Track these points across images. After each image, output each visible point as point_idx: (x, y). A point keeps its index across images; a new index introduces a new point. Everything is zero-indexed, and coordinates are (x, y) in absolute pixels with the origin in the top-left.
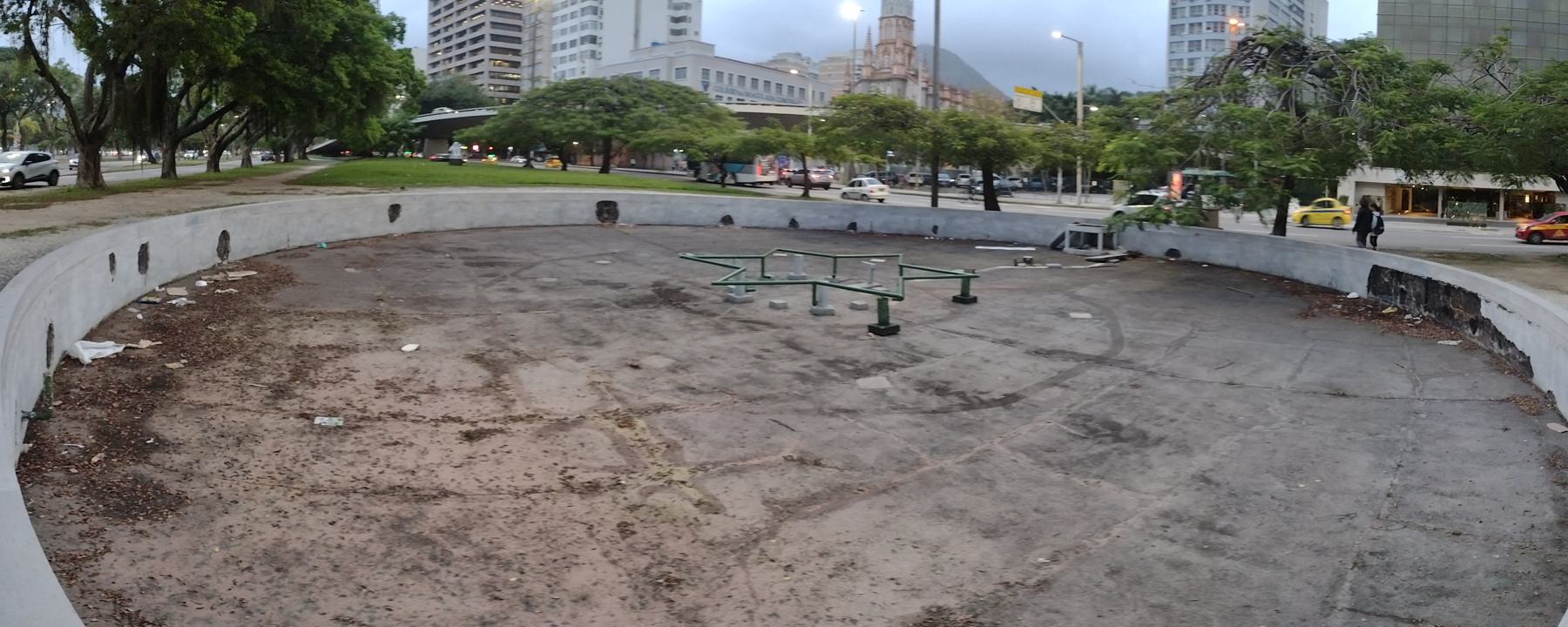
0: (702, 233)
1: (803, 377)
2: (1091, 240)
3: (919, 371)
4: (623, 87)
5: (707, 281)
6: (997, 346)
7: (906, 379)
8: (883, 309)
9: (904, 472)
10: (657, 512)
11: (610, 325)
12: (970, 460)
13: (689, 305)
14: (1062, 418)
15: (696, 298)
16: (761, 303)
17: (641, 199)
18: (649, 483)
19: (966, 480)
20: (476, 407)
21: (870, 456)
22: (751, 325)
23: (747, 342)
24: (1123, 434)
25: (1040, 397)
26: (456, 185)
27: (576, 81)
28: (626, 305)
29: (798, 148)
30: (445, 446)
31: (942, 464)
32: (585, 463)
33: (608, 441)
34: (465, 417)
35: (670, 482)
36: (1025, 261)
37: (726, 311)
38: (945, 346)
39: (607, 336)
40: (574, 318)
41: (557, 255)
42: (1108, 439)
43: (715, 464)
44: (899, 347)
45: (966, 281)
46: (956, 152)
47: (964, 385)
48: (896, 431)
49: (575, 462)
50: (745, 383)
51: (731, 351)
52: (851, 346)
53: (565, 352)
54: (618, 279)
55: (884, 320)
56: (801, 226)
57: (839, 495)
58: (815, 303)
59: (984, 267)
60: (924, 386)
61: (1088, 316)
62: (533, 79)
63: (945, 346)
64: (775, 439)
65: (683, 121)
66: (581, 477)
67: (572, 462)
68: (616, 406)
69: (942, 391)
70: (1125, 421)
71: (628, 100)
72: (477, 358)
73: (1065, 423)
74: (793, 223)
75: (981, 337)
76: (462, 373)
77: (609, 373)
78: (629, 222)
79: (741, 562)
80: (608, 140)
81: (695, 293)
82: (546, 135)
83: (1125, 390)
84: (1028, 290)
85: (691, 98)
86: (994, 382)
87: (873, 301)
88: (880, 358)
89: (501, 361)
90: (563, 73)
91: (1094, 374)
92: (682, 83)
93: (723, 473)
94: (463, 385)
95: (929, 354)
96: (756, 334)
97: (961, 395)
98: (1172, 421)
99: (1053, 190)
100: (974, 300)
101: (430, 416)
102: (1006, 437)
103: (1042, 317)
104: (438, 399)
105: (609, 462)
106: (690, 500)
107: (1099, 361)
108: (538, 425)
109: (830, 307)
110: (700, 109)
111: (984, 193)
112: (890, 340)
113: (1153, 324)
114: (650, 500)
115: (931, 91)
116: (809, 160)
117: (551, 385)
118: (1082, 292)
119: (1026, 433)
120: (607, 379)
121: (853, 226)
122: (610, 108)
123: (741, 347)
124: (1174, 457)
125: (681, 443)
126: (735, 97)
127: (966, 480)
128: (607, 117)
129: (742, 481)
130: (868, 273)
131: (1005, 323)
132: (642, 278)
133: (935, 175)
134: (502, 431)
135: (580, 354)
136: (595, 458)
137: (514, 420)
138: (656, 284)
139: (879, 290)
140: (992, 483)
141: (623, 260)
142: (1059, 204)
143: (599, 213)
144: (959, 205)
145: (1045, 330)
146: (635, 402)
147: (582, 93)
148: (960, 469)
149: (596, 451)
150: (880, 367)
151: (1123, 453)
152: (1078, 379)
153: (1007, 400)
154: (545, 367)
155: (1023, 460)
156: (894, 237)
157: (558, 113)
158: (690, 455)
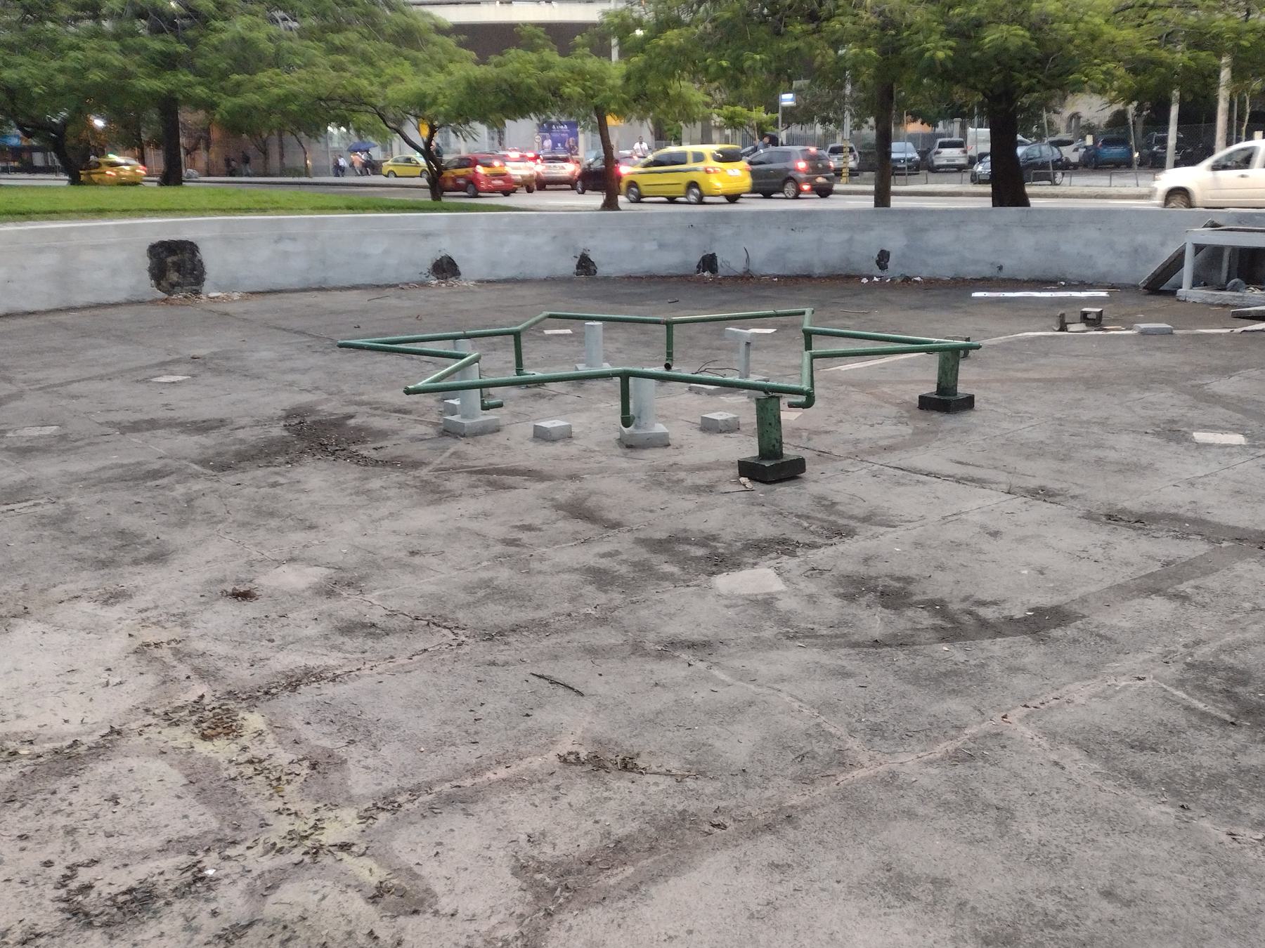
0: (391, 300)
1: (601, 578)
3: (843, 556)
6: (1018, 501)
7: (815, 572)
9: (805, 780)
11: (186, 513)
12: (957, 758)
13: (366, 451)
14: (1173, 671)
15: (382, 434)
16: (515, 433)
17: (244, 237)
18: (268, 863)
21: (738, 744)
22: (495, 478)
25: (1121, 618)
28: (221, 465)
31: (892, 764)
32: (121, 844)
33: (176, 778)
35: (316, 851)
36: (1085, 317)
37: (447, 459)
38: (905, 501)
39: (178, 538)
40: (94, 510)
41: (57, 375)
43: (414, 792)
45: (952, 357)
47: (941, 586)
51: (454, 535)
52: (701, 507)
53: (73, 588)
54: (207, 410)
55: (770, 448)
56: (602, 271)
58: (626, 422)
60: (855, 588)
61: (1238, 439)
63: (905, 501)
64: (543, 717)
66: (111, 881)
68: (199, 689)
69: (894, 596)
73: (1181, 684)
74: (585, 265)
75: (981, 482)
77: (183, 619)
81: (378, 423)
84: (1093, 383)
86: (1011, 580)
87: (740, 408)
88: (763, 529)
95: (867, 519)
96: (507, 496)
97: (937, 606)
100: (968, 403)
102: (1041, 710)
103: (1125, 441)
105: (178, 828)
106: (359, 888)
109: (660, 428)
111: (994, 179)
112: (784, 493)
114: (271, 909)
118: (1221, 386)
119: (1085, 700)
120: (178, 632)
121: (709, 262)
123: (475, 525)
125: (342, 753)
128: (156, 45)
129: (472, 823)
131: (1036, 451)
132: (258, 403)
133: (885, 139)
135: (111, 586)
138: (289, 414)
140: (1004, 816)
141: (217, 371)
143: (158, 273)
144: (946, 202)
146: (242, 675)
148: (932, 777)
150: (761, 548)
152: (1213, 582)
153: (1041, 623)
155: (1077, 764)
156: (797, 281)
157: (37, 42)
158: (362, 781)
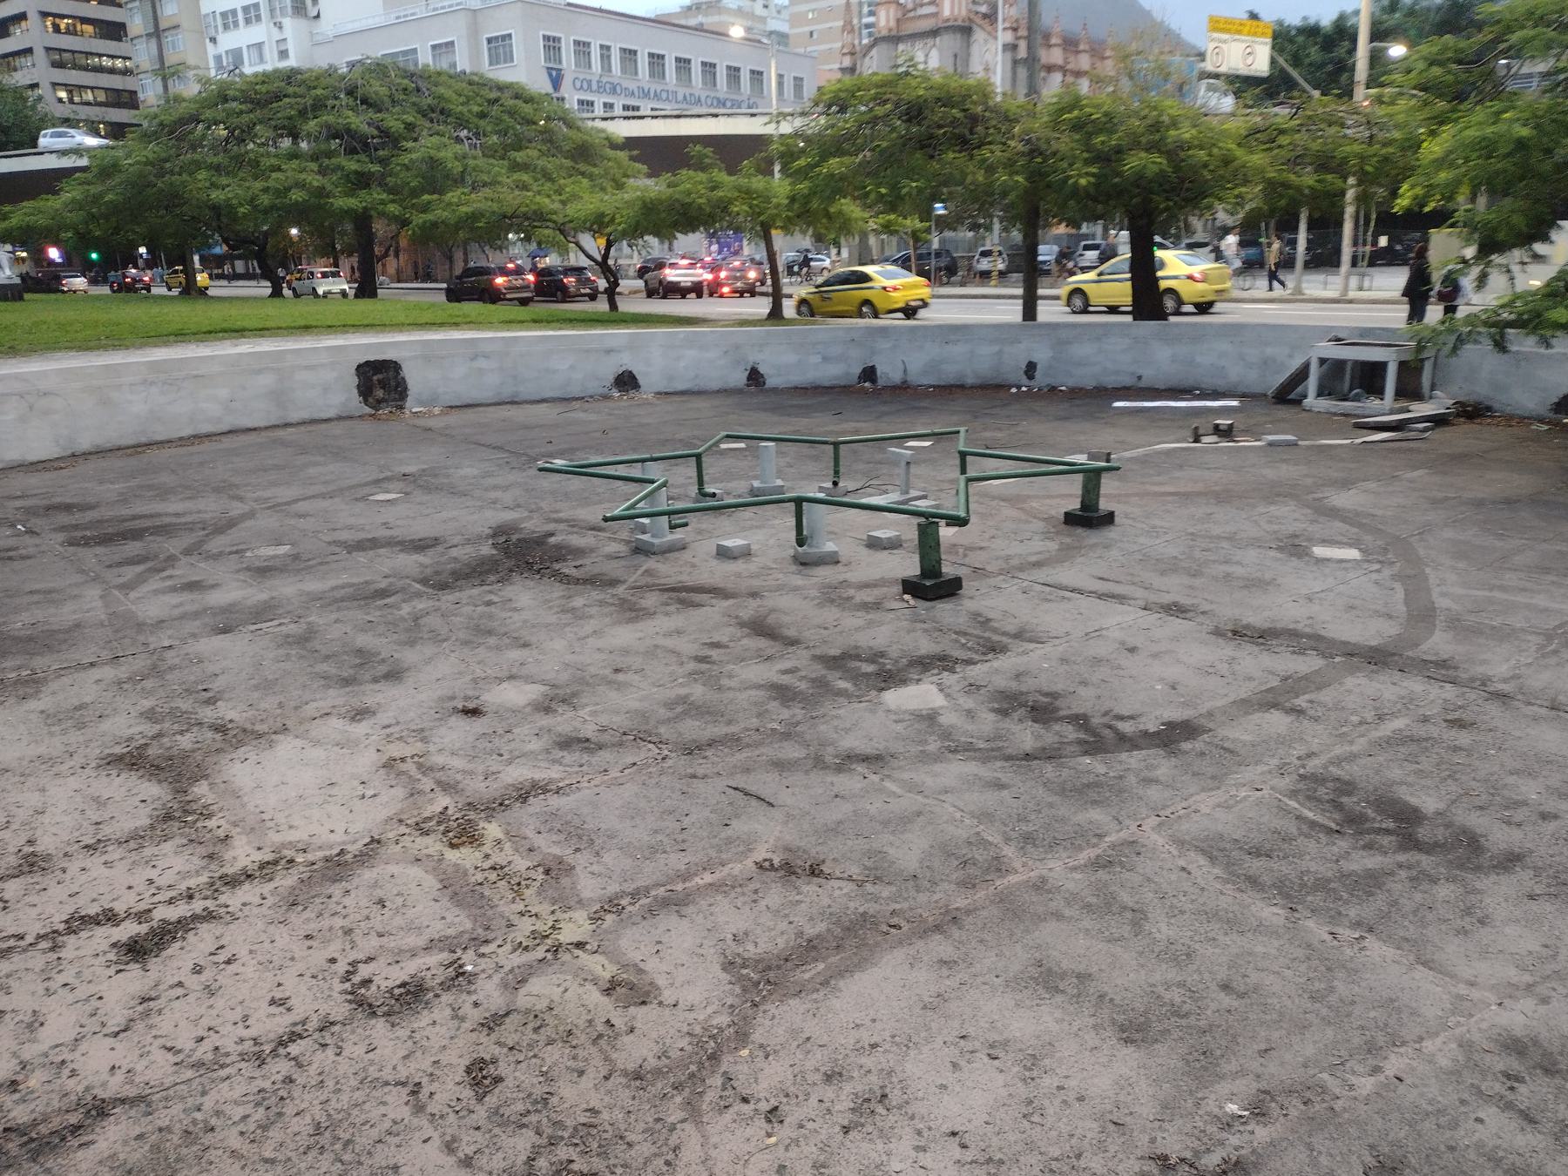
0: (578, 414)
1: (783, 694)
2: (1369, 378)
3: (997, 671)
4: (378, 89)
5: (593, 514)
6: (1152, 618)
7: (973, 688)
8: (928, 543)
10: (536, 1020)
11: (413, 632)
12: (1098, 864)
13: (567, 569)
14: (1286, 782)
15: (579, 552)
16: (700, 550)
18: (518, 959)
19: (1088, 907)
20: (140, 877)
21: (908, 852)
22: (685, 595)
23: (679, 632)
24: (1423, 833)
25: (1241, 732)
26: (85, 346)
27: (266, 78)
28: (441, 583)
29: (755, 214)
30: (82, 992)
33: (432, 883)
34: (120, 908)
35: (556, 949)
36: (1217, 430)
37: (636, 576)
38: (1051, 617)
39: (409, 656)
40: (337, 628)
41: (285, 493)
42: (1386, 840)
43: (635, 895)
44: (962, 621)
45: (1092, 479)
46: (1076, 192)
47: (1085, 701)
48: (955, 798)
49: (368, 945)
50: (677, 718)
51: (652, 652)
53: (324, 705)
55: (931, 568)
56: (771, 382)
57: (852, 941)
58: (801, 542)
60: (1008, 703)
61: (1353, 554)
62: (165, 72)
63: (1051, 617)
64: (739, 827)
65: (516, 167)
69: (1042, 711)
70: (1429, 803)
71: (393, 123)
72: (132, 760)
73: (1293, 794)
74: (755, 377)
75: (1120, 598)
76: (100, 803)
78: (430, 402)
79: (693, 1111)
80: (362, 221)
81: (576, 540)
82: (220, 216)
83: (1434, 731)
84: (1222, 497)
85: (527, 109)
86: (1146, 697)
87: (908, 529)
88: (926, 646)
89: (185, 755)
90: (237, 55)
91: (1361, 688)
92: (504, 75)
93: (651, 912)
94: (107, 830)
95: (1019, 635)
97: (1080, 721)
98: (1544, 816)
100: (1109, 518)
101: (33, 929)
102: (1174, 818)
103: (1251, 555)
104: (49, 881)
105: (437, 929)
107: (1376, 658)
108: (286, 881)
109: (830, 547)
110: (548, 137)
112: (944, 610)
113: (1510, 578)
115: (1022, 52)
116: (776, 234)
117: (303, 785)
118: (1343, 499)
120: (419, 747)
121: (869, 374)
122: (356, 143)
123: (669, 643)
124: (1547, 907)
125: (570, 860)
126: (618, 104)
127: (1088, 907)
128: (352, 165)
130: (901, 470)
131: (1169, 567)
132: (466, 522)
133: (1032, 250)
134: (209, 916)
135: (356, 702)
136: (410, 928)
137: (232, 882)
138: (500, 531)
139: (922, 505)
140: (1138, 917)
141: (428, 489)
142: (1298, 298)
143: (365, 391)
145: (1255, 584)
146: (478, 788)
147: (286, 108)
148: (1076, 882)
149: (409, 909)
151: (1420, 878)
152: (1326, 696)
153: (1173, 736)
154: (287, 747)
155: (1197, 862)
156: (949, 391)
157: (239, 161)
158: (589, 887)
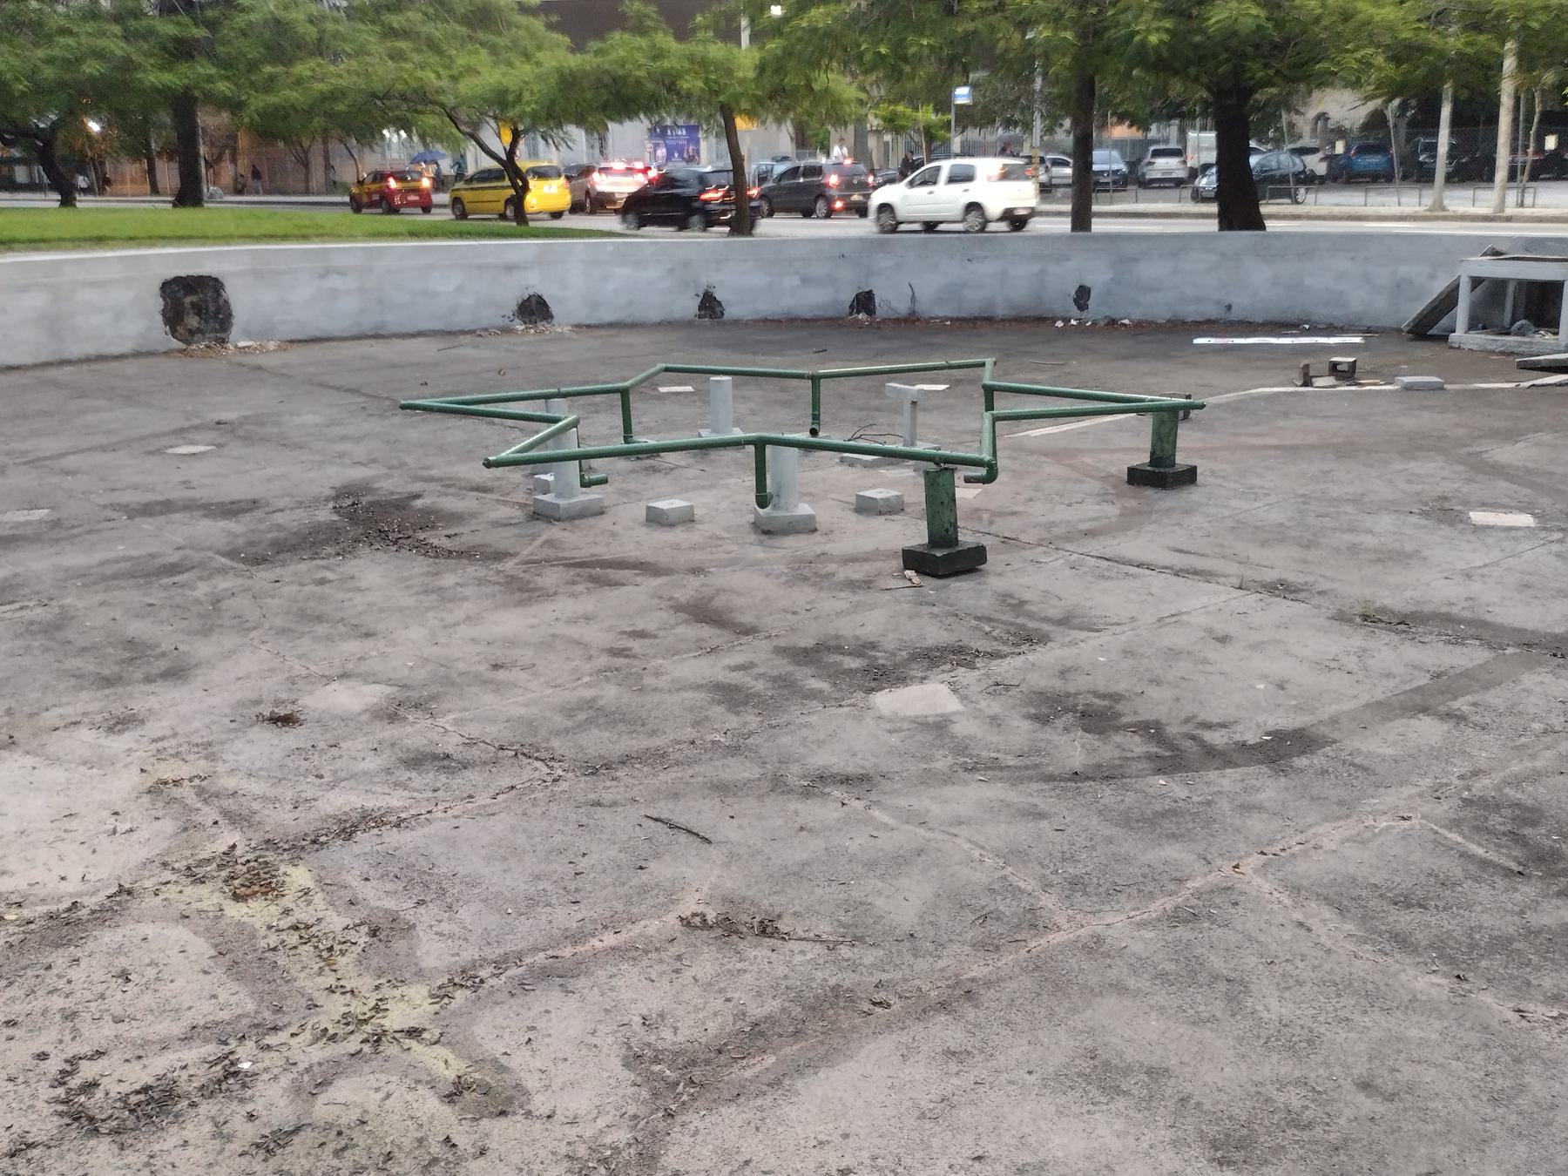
0: (467, 350)
1: (731, 696)
3: (1035, 668)
7: (999, 687)
8: (939, 502)
11: (211, 617)
13: (437, 538)
14: (1444, 808)
15: (456, 518)
18: (318, 1053)
21: (903, 902)
22: (599, 572)
23: (587, 618)
25: (1379, 744)
28: (254, 557)
31: (1094, 926)
32: (133, 1031)
33: (201, 948)
36: (1334, 369)
37: (539, 549)
39: (203, 649)
40: (97, 614)
41: (49, 446)
43: (500, 965)
44: (986, 604)
45: (1169, 419)
47: (1157, 704)
51: (548, 644)
52: (856, 608)
53: (69, 711)
54: (235, 489)
56: (731, 312)
57: (820, 1022)
58: (762, 501)
59: (1219, 390)
60: (1048, 707)
61: (1526, 520)
64: (660, 870)
65: (391, 33)
66: (122, 1077)
67: (96, 1034)
68: (229, 837)
69: (1097, 718)
73: (1455, 824)
74: (709, 304)
75: (1206, 575)
77: (208, 750)
78: (265, 333)
81: (450, 503)
84: (1345, 450)
87: (905, 483)
88: (935, 635)
93: (523, 986)
95: (1065, 621)
96: (614, 596)
97: (1152, 730)
99: (1421, 175)
100: (1189, 477)
102: (1285, 857)
103: (1386, 521)
105: (204, 1011)
109: (804, 509)
112: (961, 590)
114: (321, 1110)
118: (1504, 454)
119: (1336, 846)
121: (864, 301)
123: (573, 631)
125: (410, 917)
129: (573, 1002)
131: (1273, 536)
132: (299, 477)
135: (118, 709)
138: (341, 493)
140: (1236, 989)
141: (248, 440)
142: (1438, 213)
143: (173, 317)
144: (1162, 224)
146: (283, 820)
148: (1145, 943)
150: (932, 658)
153: (1281, 750)
155: (1322, 918)
158: (434, 951)
